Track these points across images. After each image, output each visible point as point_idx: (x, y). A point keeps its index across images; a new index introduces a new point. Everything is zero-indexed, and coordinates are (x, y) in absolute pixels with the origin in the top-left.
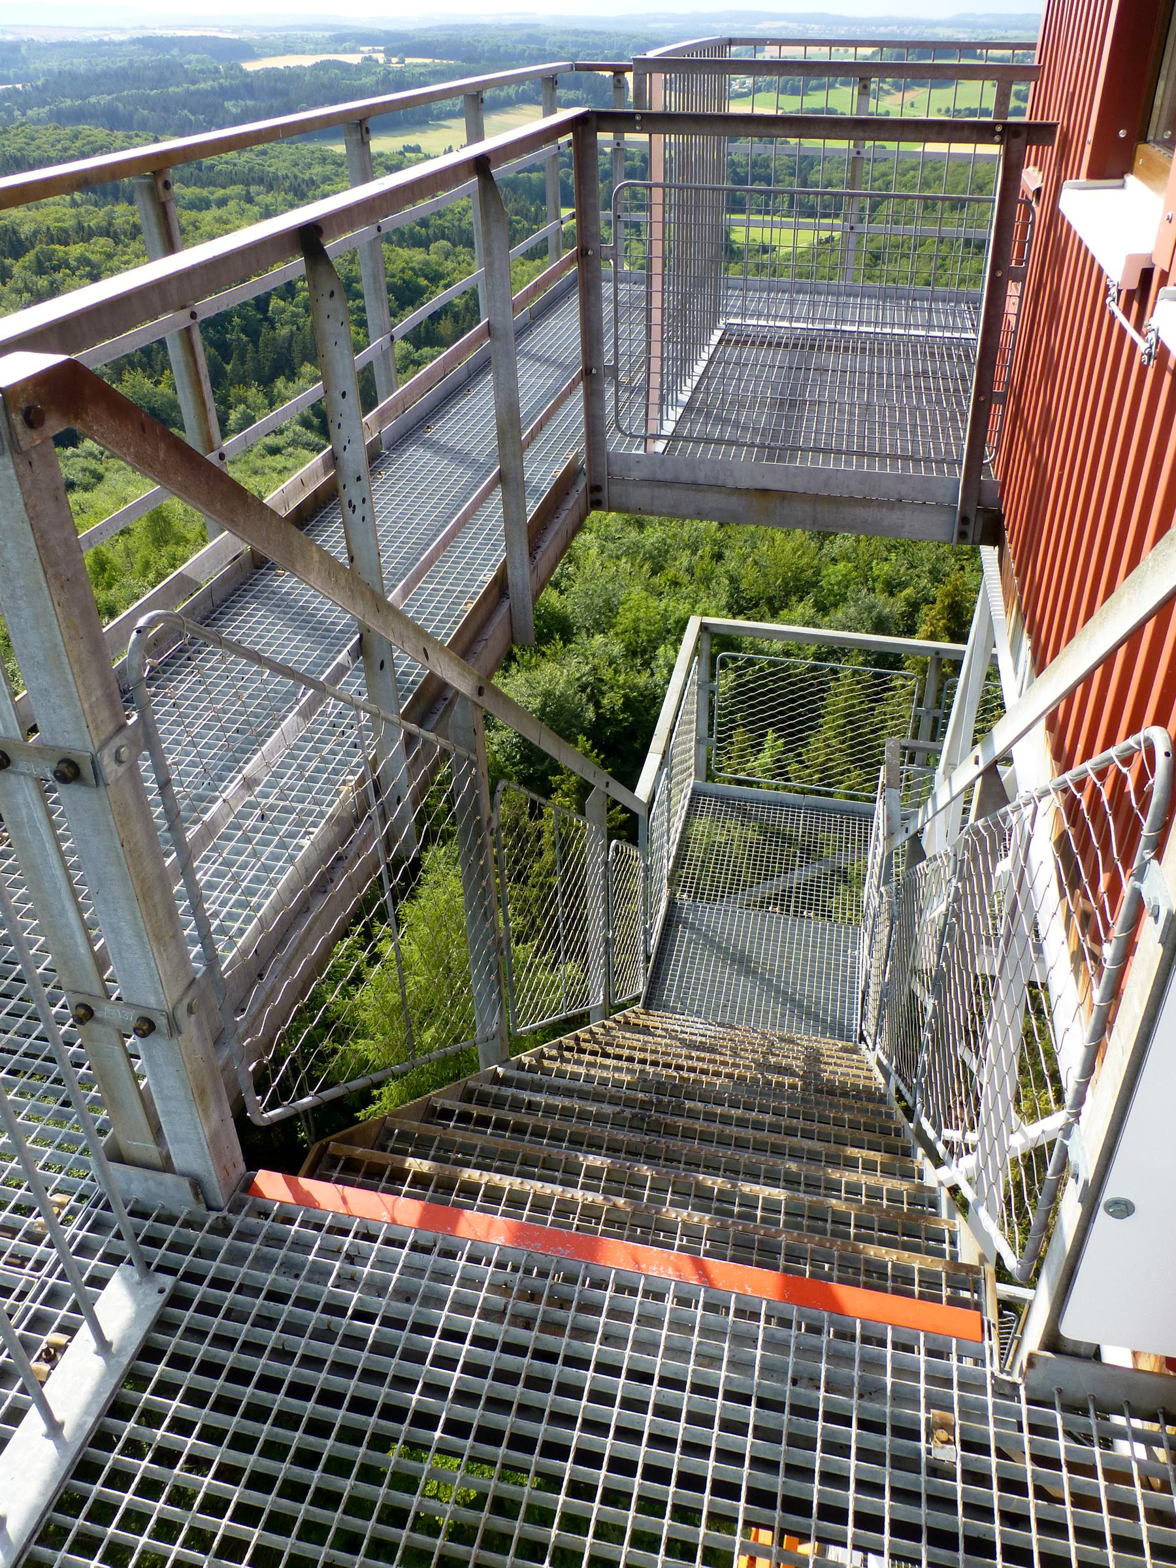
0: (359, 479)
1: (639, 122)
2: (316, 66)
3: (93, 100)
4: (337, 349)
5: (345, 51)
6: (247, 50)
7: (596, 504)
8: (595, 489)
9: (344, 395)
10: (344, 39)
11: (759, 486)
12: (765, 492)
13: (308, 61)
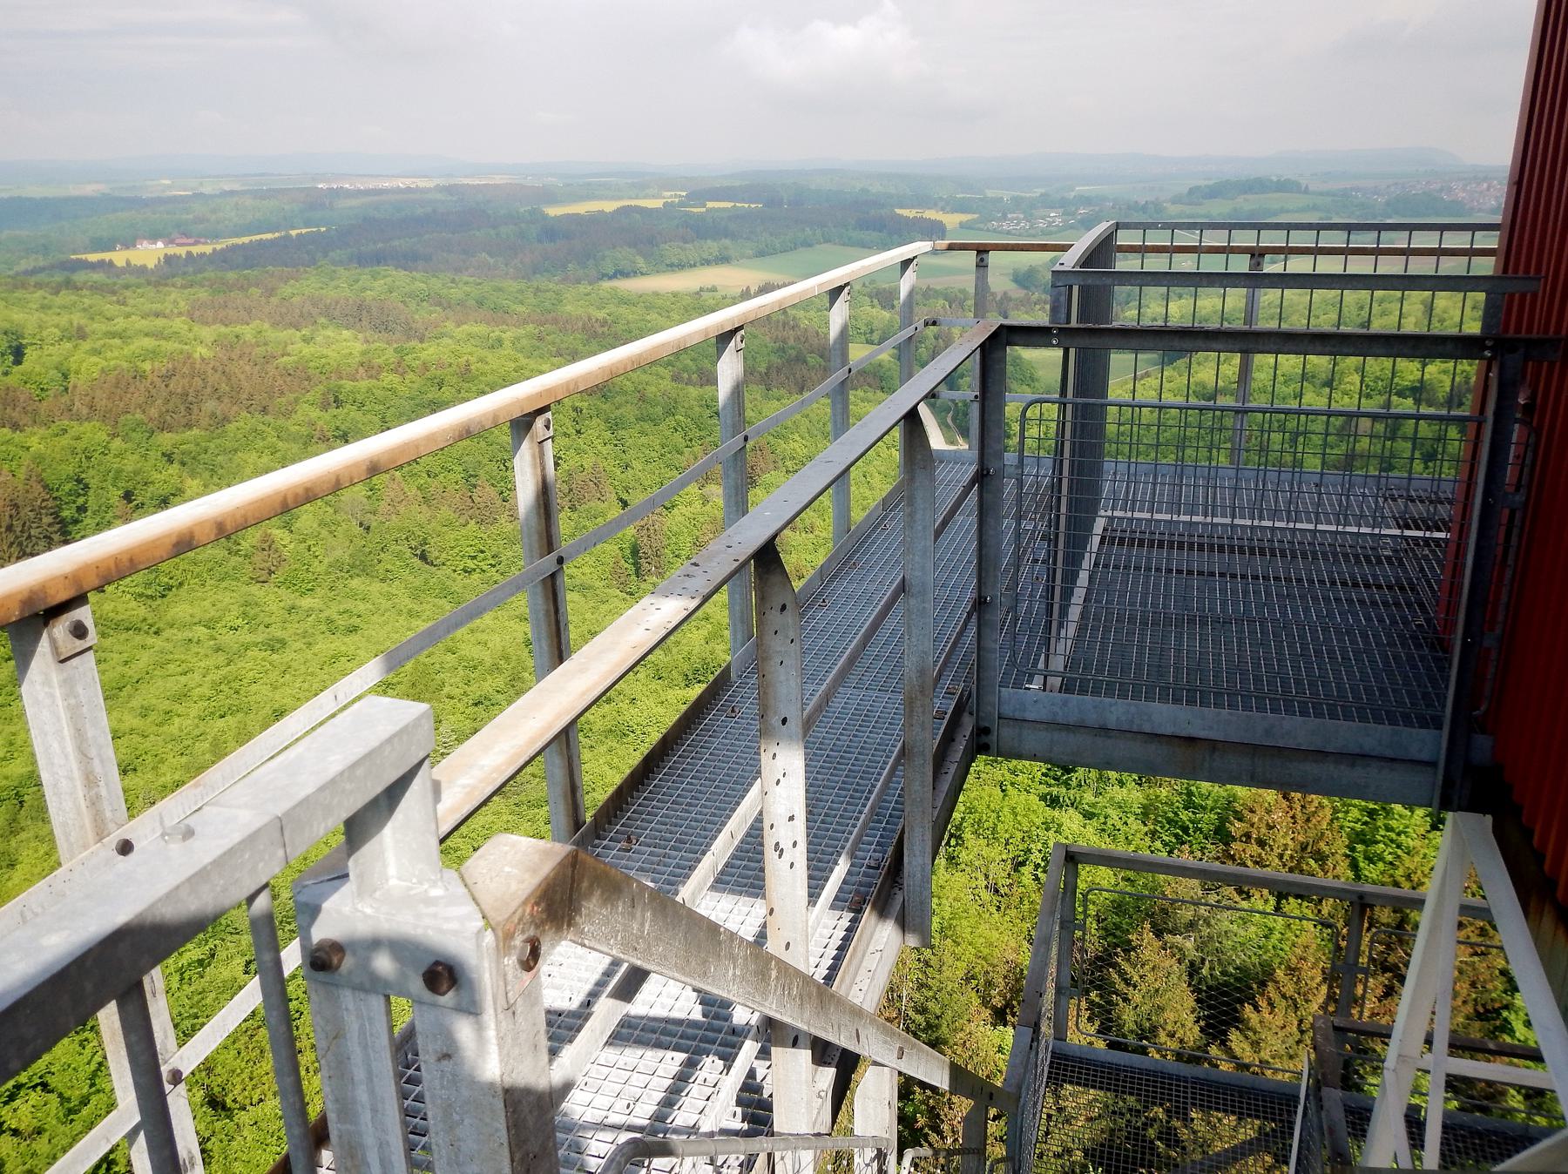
0: (791, 818)
1: (1056, 335)
2: (619, 211)
3: (396, 243)
4: (781, 670)
5: (645, 197)
6: (551, 197)
7: (984, 749)
8: (982, 731)
9: (784, 721)
10: (642, 184)
11: (1184, 734)
12: (1191, 740)
13: (609, 206)
